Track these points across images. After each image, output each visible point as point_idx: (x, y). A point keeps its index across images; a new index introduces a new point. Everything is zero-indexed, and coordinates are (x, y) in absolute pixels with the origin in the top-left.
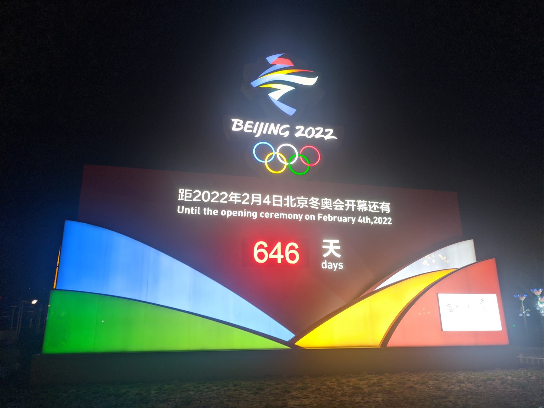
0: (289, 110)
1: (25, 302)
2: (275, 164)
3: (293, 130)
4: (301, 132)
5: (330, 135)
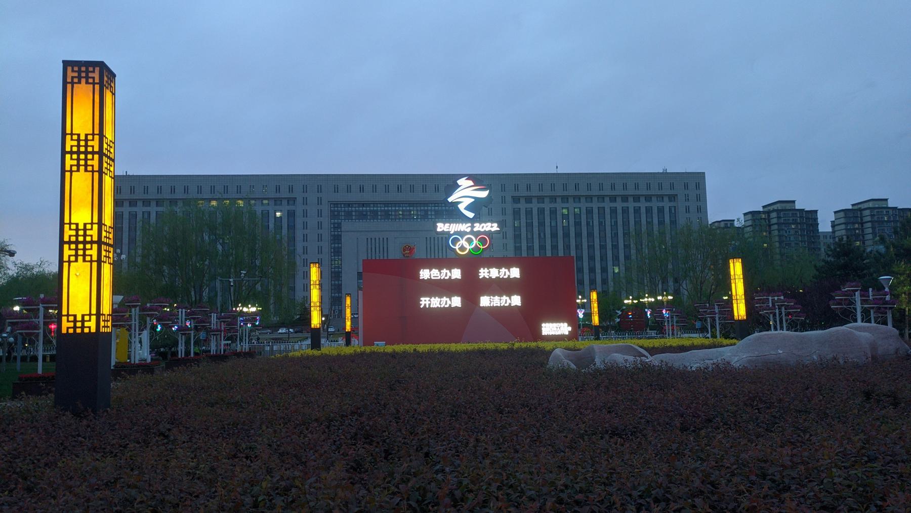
0: (471, 215)
1: (198, 318)
2: (462, 248)
3: (473, 227)
4: (478, 227)
5: (495, 227)
